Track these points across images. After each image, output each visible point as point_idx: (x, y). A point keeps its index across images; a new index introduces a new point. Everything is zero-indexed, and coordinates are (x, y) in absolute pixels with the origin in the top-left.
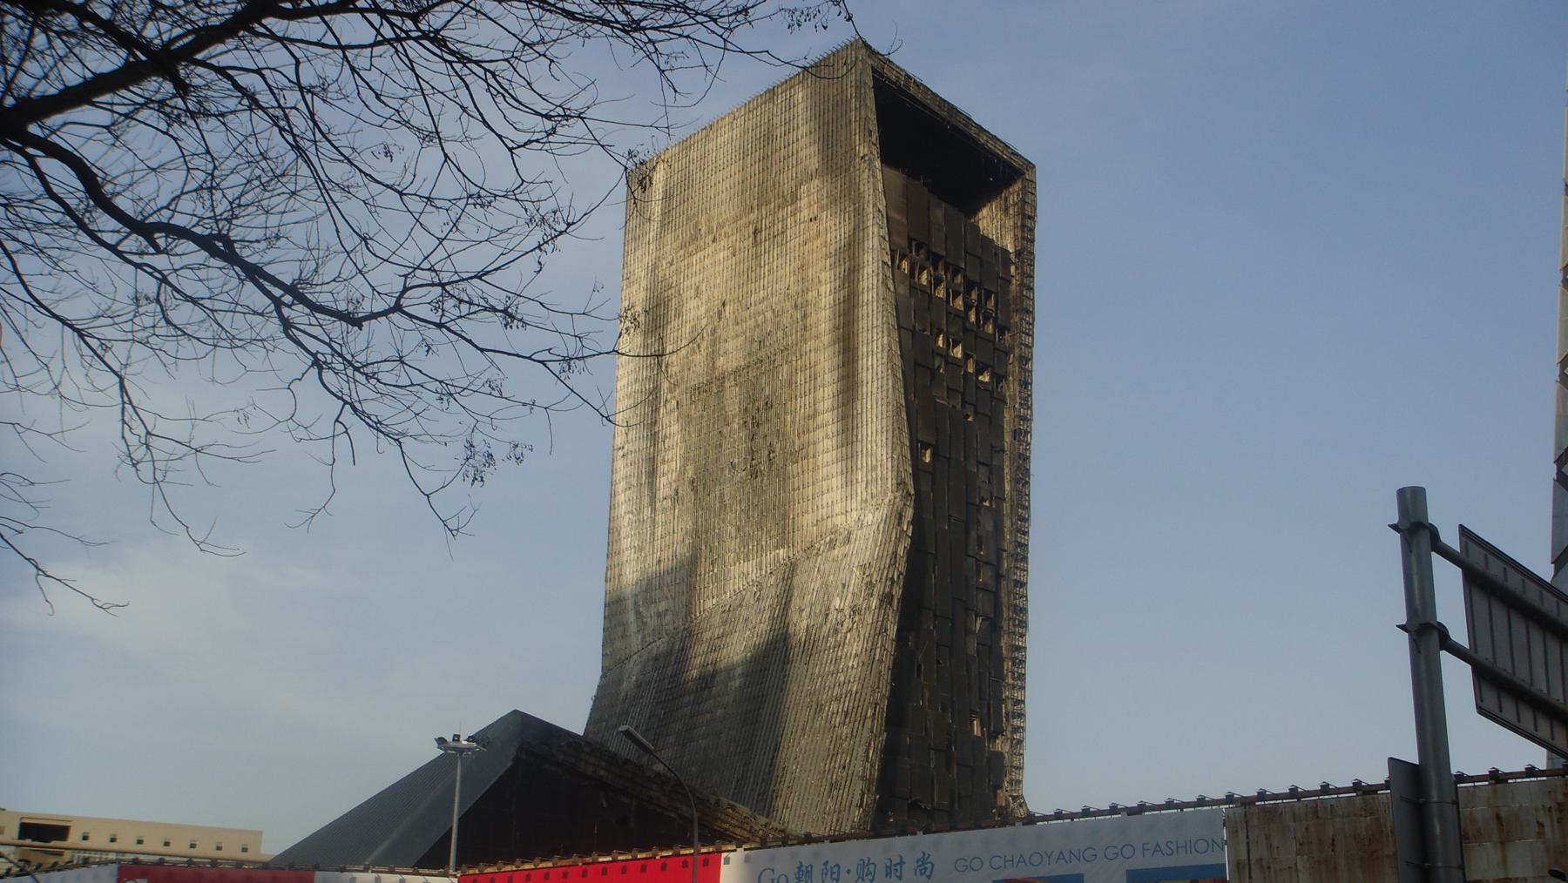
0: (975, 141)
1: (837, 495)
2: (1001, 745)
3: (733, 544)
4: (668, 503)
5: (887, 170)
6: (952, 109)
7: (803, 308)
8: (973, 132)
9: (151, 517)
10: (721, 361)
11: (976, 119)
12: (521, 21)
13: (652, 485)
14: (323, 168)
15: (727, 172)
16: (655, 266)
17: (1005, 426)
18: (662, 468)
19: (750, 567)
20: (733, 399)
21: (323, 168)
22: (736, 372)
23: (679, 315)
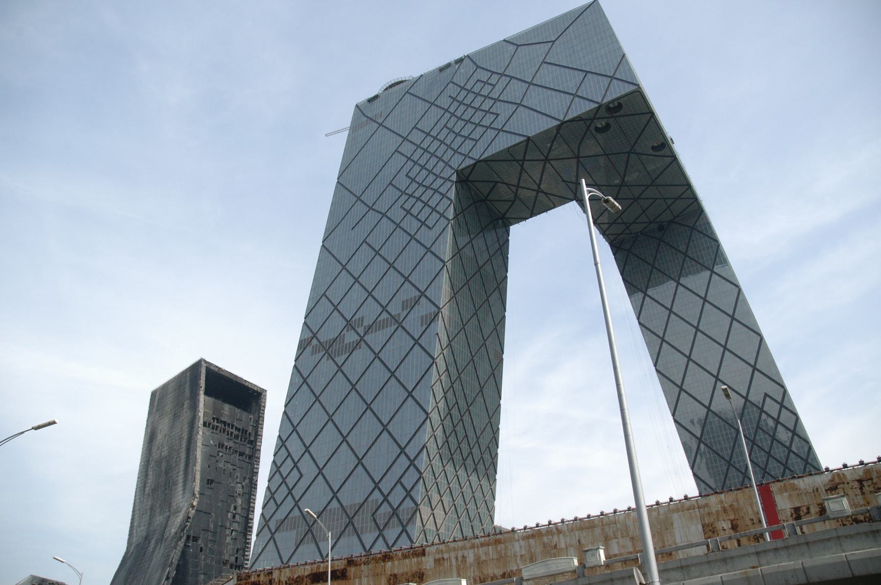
0: (244, 385)
1: (180, 497)
2: (321, 581)
3: (158, 510)
4: (147, 496)
5: (207, 398)
6: (236, 377)
7: (181, 438)
8: (243, 383)
9: (299, 479)
10: (163, 454)
11: (244, 378)
12: (643, 188)
13: (144, 490)
14: (596, 264)
15: (171, 395)
16: (153, 422)
17: (199, 482)
18: (147, 485)
19: (161, 517)
20: (164, 465)
21: (596, 264)
22: (166, 457)
23: (156, 438)
